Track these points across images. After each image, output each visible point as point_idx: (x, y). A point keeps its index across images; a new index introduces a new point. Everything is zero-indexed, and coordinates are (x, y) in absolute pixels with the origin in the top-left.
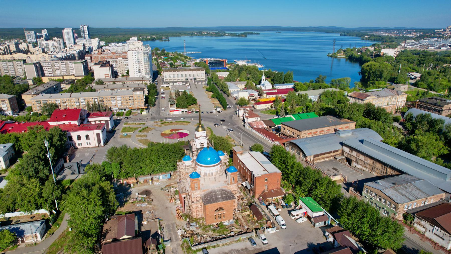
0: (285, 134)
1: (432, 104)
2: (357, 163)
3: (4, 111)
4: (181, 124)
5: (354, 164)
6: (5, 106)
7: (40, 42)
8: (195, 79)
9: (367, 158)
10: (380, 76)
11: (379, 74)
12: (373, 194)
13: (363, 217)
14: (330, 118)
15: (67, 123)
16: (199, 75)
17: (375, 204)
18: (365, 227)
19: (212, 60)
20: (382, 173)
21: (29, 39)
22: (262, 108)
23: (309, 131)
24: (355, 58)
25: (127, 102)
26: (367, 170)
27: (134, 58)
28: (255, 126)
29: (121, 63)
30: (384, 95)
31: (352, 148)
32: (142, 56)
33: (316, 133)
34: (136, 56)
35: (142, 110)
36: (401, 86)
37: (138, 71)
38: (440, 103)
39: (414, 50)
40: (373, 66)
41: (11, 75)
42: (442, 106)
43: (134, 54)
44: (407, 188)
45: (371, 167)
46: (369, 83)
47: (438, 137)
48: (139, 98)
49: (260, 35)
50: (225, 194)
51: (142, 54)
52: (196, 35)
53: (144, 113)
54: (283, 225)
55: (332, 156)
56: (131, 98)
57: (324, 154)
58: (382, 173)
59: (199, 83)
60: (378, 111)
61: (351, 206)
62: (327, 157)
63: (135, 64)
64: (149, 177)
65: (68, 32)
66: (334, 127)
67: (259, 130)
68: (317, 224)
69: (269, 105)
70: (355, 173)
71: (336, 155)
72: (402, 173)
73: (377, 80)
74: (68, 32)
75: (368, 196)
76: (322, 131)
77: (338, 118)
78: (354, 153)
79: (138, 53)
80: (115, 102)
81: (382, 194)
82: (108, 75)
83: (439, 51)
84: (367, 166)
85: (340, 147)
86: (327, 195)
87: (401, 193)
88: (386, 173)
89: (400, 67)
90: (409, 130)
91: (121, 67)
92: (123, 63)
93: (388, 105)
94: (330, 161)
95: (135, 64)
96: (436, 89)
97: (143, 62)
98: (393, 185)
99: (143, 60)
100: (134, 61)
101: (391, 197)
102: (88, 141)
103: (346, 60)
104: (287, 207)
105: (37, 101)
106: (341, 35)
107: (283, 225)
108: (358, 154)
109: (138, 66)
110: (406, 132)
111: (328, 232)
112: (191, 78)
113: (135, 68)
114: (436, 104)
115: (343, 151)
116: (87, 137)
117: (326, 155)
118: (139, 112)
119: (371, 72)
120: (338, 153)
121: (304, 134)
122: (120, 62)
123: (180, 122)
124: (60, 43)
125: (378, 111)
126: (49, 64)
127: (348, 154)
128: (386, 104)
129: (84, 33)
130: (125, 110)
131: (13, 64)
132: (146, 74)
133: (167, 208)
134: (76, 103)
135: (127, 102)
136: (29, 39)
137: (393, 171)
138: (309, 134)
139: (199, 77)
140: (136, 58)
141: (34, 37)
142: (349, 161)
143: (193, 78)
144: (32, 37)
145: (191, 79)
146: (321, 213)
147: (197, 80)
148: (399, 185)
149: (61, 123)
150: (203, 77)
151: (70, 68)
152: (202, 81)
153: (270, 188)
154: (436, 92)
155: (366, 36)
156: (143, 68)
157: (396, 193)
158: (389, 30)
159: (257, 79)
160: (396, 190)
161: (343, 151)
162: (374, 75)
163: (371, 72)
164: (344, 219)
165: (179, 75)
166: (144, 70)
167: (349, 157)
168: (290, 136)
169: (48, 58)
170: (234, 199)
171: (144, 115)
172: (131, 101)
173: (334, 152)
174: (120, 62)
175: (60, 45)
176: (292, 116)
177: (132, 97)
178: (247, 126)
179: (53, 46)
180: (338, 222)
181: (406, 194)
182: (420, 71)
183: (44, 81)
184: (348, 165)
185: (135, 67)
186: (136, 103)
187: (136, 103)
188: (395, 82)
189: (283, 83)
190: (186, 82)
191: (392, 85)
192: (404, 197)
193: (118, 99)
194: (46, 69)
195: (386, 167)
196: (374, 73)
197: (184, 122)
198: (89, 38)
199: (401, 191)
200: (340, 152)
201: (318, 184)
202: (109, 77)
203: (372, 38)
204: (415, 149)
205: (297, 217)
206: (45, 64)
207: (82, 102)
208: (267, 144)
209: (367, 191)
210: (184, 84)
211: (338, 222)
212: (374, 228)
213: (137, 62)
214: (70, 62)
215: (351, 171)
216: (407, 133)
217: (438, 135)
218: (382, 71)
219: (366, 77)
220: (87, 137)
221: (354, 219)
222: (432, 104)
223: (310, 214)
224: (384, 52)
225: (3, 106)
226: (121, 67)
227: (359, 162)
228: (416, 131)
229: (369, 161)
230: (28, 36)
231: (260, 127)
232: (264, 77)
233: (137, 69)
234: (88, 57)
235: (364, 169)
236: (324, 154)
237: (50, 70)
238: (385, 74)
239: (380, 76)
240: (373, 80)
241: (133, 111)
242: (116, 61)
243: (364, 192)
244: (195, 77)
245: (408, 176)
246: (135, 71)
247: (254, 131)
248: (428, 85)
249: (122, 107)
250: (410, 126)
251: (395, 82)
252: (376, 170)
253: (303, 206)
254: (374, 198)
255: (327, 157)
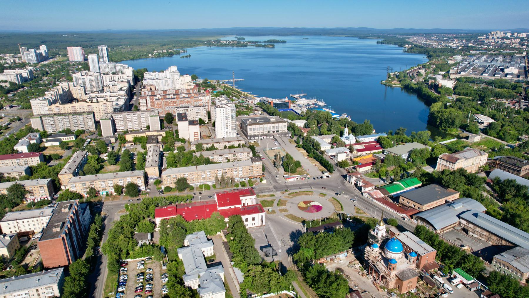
0: (404, 204)
1: (511, 164)
2: (474, 233)
3: (139, 186)
4: (306, 194)
5: (471, 234)
6: (140, 182)
7: (76, 78)
8: (277, 131)
9: (483, 231)
10: (453, 124)
11: (451, 121)
12: (502, 264)
13: (509, 286)
14: (436, 187)
15: (233, 207)
16: (281, 127)
17: (504, 271)
18: (511, 292)
19: (277, 101)
20: (498, 243)
21: (28, 58)
22: (363, 170)
23: (428, 204)
24: (412, 88)
25: (247, 171)
26: (483, 239)
27: (222, 115)
28: (375, 196)
29: (192, 112)
30: (470, 157)
31: (468, 222)
32: (230, 112)
33: (432, 205)
34: (224, 113)
35: (261, 180)
36: (475, 137)
37: (225, 127)
38: (518, 164)
39: (469, 78)
40: (444, 113)
41: (81, 129)
42: (521, 168)
43: (222, 111)
44: (525, 260)
45: (487, 238)
46: (440, 129)
47: (525, 202)
48: (257, 167)
49: (287, 45)
50: (413, 272)
51: (230, 111)
52: (215, 45)
53: (264, 182)
54: (452, 291)
55: (452, 227)
56: (251, 168)
57: (448, 226)
58: (498, 243)
59: (283, 136)
60: (472, 178)
61: (499, 278)
62: (449, 229)
63: (223, 121)
64: (333, 257)
65: (93, 59)
66: (445, 199)
67: (379, 199)
68: (472, 289)
69: (368, 168)
70: (475, 242)
71: (455, 226)
72: (515, 246)
73: (449, 127)
74: (93, 59)
75: (497, 265)
76: (437, 203)
77: (443, 187)
78: (471, 226)
79: (226, 110)
80: (237, 173)
81: (509, 265)
82: (198, 132)
83: (493, 78)
84: (483, 236)
85: (457, 220)
86: (474, 268)
87: (522, 264)
88: (501, 244)
89: (470, 114)
90: (498, 193)
91: (192, 115)
92: (194, 112)
93: (473, 164)
94: (451, 231)
95: (223, 121)
96: (506, 139)
97: (230, 118)
98: (515, 258)
99: (230, 116)
100: (222, 117)
101: (518, 268)
102: (253, 222)
103: (402, 89)
104: (445, 276)
105: (168, 176)
106: (378, 43)
107: (452, 291)
108: (475, 227)
109: (226, 122)
110: (496, 195)
111: (483, 295)
112: (274, 130)
113: (223, 125)
114: (515, 165)
115: (460, 223)
116: (253, 219)
117: (449, 227)
118: (258, 180)
119: (443, 119)
120: (456, 224)
121: (425, 207)
122: (192, 110)
123: (304, 192)
124: (97, 78)
125: (472, 178)
126: (121, 116)
127: (465, 225)
128: (471, 164)
129: (103, 54)
130: (245, 179)
131: (83, 117)
132: (232, 130)
133: (364, 282)
134: (203, 175)
135: (247, 171)
136: (28, 58)
137: (508, 243)
138: (428, 206)
139: (281, 129)
140: (225, 115)
141: (33, 56)
142: (466, 231)
143: (275, 130)
144: (32, 56)
145: (274, 132)
146: (472, 281)
147: (279, 132)
148: (519, 258)
149: (228, 207)
150: (285, 129)
151: (142, 120)
152: (285, 134)
153: (429, 262)
154: (506, 141)
155: (407, 46)
156: (230, 124)
157: (520, 265)
158: (427, 34)
159: (338, 130)
160: (519, 262)
161: (460, 223)
162: (445, 122)
163: (443, 119)
164: (494, 287)
165: (259, 129)
166: (231, 126)
167: (466, 227)
168: (410, 207)
169: (109, 106)
170: (477, 290)
171: (264, 185)
172: (251, 171)
173: (454, 224)
174: (192, 110)
175: (98, 80)
176: (400, 184)
177: (252, 167)
178: (366, 195)
179: (90, 81)
180: (488, 288)
181: (526, 265)
182: (485, 114)
183: (127, 139)
184: (465, 233)
185: (223, 123)
186: (255, 172)
187: (255, 172)
188: (467, 129)
189: (364, 135)
190: (270, 136)
191: (463, 132)
192: (525, 267)
193: (240, 170)
194: (117, 122)
195: (501, 240)
196: (446, 120)
197: (308, 192)
198: (109, 62)
199: (523, 263)
200: (458, 223)
201: (466, 260)
202: (198, 134)
203: (415, 49)
204: (519, 223)
205: (456, 284)
206: (116, 116)
207: (208, 175)
208: (388, 212)
209: (496, 262)
210: (268, 137)
211: (488, 288)
212: (517, 294)
213: (225, 119)
214: (143, 114)
215: (472, 241)
216: (497, 196)
217: (525, 200)
218: (455, 119)
219: (438, 123)
220: (253, 219)
221: (502, 287)
222: (511, 164)
223: (465, 281)
224: (443, 84)
225: (138, 182)
226: (192, 115)
227: (476, 232)
228: (506, 196)
229: (485, 233)
230: (27, 54)
231: (379, 196)
232: (346, 130)
233: (225, 125)
234: (143, 100)
235: (480, 238)
236: (448, 226)
237: (122, 123)
238: (457, 122)
239: (453, 124)
240: (445, 127)
241: (253, 180)
242: (187, 110)
243: (494, 262)
244: (277, 130)
245: (522, 249)
246: (223, 127)
247: (374, 201)
248: (498, 134)
249: (243, 176)
250: (498, 188)
251: (467, 129)
252: (491, 240)
253: (458, 275)
254: (502, 267)
255: (449, 229)
